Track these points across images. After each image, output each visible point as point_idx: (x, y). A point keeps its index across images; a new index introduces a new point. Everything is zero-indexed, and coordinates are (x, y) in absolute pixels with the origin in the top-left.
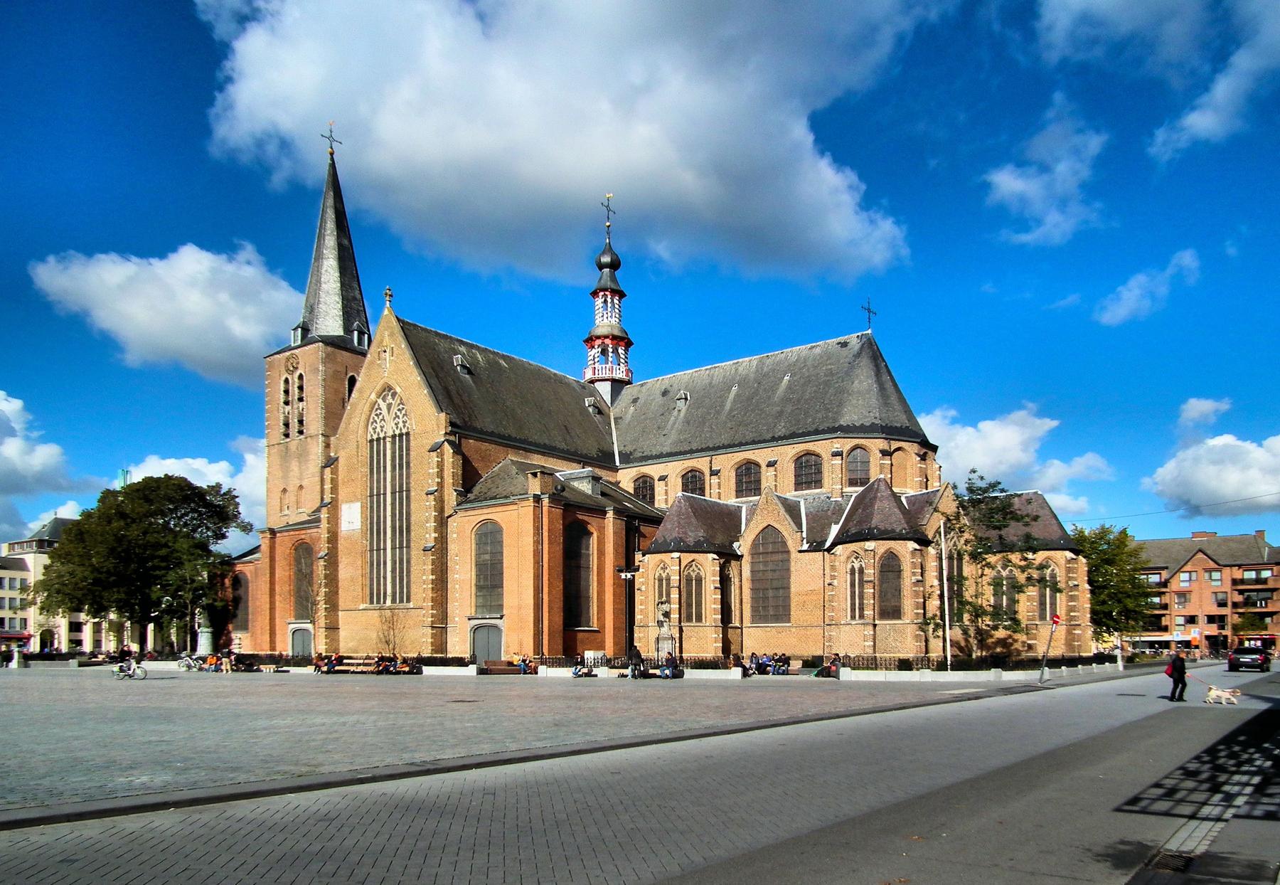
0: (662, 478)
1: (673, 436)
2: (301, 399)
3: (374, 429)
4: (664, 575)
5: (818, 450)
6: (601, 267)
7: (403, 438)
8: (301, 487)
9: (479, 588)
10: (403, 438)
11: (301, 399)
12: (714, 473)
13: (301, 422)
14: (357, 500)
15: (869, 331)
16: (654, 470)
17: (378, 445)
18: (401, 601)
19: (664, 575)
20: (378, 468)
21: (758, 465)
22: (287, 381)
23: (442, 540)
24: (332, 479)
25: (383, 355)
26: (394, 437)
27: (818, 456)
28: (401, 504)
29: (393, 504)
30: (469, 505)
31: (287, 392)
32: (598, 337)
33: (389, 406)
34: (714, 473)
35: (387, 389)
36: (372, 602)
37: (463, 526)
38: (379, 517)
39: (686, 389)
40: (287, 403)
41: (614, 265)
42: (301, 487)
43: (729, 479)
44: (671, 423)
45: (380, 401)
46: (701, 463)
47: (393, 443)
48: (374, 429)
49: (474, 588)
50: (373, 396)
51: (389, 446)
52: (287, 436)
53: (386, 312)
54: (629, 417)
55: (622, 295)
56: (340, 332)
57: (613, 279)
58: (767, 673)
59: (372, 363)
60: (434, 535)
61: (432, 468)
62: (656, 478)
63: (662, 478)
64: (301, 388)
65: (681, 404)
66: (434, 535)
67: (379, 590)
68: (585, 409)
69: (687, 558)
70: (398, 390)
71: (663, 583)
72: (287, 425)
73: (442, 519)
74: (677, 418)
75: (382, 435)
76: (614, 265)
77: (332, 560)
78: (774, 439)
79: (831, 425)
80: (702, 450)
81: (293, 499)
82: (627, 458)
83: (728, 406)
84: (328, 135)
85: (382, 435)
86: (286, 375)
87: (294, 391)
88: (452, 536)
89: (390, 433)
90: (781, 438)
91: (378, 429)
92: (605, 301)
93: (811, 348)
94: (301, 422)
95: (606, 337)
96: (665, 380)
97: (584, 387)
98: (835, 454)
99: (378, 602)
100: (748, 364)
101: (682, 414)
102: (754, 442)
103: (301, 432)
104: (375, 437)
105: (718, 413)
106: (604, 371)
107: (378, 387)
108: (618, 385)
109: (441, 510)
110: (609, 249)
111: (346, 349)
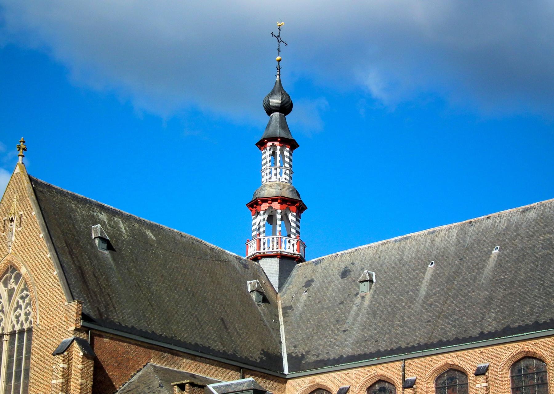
1: (356, 333)
6: (270, 110)
25: (9, 225)
26: (13, 334)
27: (541, 360)
32: (265, 200)
41: (285, 108)
44: (352, 314)
55: (293, 145)
65: (364, 288)
70: (23, 270)
74: (360, 308)
78: (483, 336)
83: (423, 290)
89: (9, 329)
92: (274, 154)
95: (274, 200)
96: (345, 256)
97: (246, 266)
101: (367, 303)
102: (457, 341)
105: (412, 300)
108: (288, 262)
110: (279, 89)
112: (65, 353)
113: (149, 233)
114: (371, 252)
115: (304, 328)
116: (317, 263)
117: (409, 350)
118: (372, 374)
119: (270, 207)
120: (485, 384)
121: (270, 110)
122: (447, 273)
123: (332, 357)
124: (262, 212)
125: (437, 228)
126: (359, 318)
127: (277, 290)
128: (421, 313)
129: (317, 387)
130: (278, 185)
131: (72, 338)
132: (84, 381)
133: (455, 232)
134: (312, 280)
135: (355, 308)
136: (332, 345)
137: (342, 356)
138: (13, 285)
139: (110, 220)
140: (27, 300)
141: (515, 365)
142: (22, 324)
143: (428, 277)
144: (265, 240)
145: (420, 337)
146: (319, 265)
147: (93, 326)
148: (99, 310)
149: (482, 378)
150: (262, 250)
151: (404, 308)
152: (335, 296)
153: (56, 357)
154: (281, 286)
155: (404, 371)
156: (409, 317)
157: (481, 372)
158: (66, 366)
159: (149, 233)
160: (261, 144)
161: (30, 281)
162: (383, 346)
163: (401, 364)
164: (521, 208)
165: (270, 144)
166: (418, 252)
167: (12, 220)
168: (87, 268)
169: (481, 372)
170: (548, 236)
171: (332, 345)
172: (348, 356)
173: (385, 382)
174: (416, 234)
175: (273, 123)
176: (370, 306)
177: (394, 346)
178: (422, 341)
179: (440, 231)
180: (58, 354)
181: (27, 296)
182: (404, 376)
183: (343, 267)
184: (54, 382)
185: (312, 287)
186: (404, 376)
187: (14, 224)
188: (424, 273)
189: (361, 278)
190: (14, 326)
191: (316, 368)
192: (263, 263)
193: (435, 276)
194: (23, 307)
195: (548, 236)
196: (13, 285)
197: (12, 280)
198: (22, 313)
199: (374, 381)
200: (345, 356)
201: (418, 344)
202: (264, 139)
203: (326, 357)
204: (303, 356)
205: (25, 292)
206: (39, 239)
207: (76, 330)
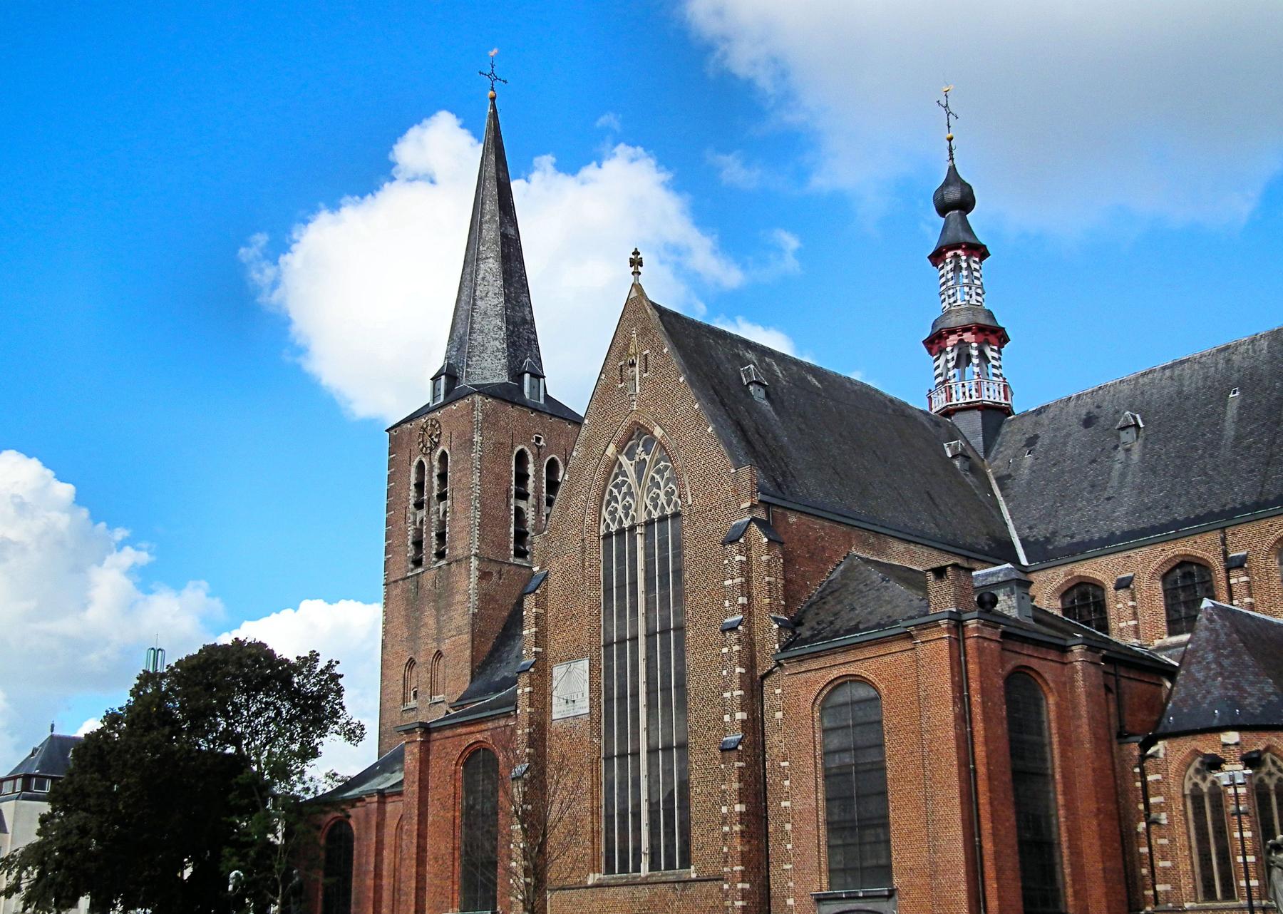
1: (1128, 500)
2: (442, 497)
3: (613, 513)
4: (1205, 787)
5: (1099, 576)
8: (439, 654)
9: (833, 827)
11: (442, 497)
12: (1233, 565)
13: (441, 537)
16: (1101, 569)
18: (670, 865)
19: (1205, 787)
21: (1098, 587)
23: (755, 727)
24: (537, 616)
26: (649, 524)
28: (666, 655)
29: (650, 659)
30: (806, 648)
31: (420, 486)
32: (952, 331)
36: (609, 869)
39: (1130, 408)
40: (419, 505)
42: (439, 654)
43: (1153, 595)
44: (1115, 474)
45: (623, 459)
46: (1203, 547)
47: (648, 536)
48: (613, 513)
49: (823, 830)
50: (611, 449)
51: (640, 542)
54: (1025, 472)
60: (740, 716)
61: (732, 583)
62: (1110, 586)
63: (1123, 584)
64: (443, 477)
66: (740, 716)
68: (949, 462)
69: (1258, 742)
70: (658, 432)
71: (1208, 809)
72: (418, 544)
73: (752, 680)
74: (1126, 466)
77: (537, 784)
81: (425, 677)
82: (1043, 553)
84: (488, 71)
89: (643, 517)
94: (441, 537)
97: (937, 424)
99: (624, 869)
101: (1135, 457)
103: (441, 555)
105: (1214, 445)
107: (620, 433)
109: (750, 664)
111: (514, 404)
112: (742, 540)
113: (810, 378)
115: (1040, 501)
118: (1170, 554)
119: (961, 341)
120: (1134, 622)
121: (943, 209)
122: (1264, 402)
124: (949, 349)
126: (1129, 478)
127: (982, 455)
128: (1235, 461)
129: (1077, 581)
130: (968, 309)
131: (747, 519)
132: (772, 579)
134: (1036, 437)
135: (1117, 466)
136: (1093, 521)
137: (1113, 533)
138: (643, 456)
139: (761, 361)
140: (667, 474)
141: (825, 704)
142: (621, 522)
143: (1232, 411)
145: (1241, 493)
146: (1044, 416)
147: (775, 502)
148: (775, 480)
150: (954, 402)
151: (1201, 457)
152: (1080, 454)
153: (728, 547)
154: (987, 450)
155: (1224, 544)
156: (1214, 469)
158: (744, 559)
159: (810, 378)
161: (671, 444)
162: (1180, 513)
165: (950, 254)
166: (1206, 378)
167: (633, 364)
168: (747, 423)
171: (1093, 521)
172: (1123, 532)
173: (1192, 563)
175: (952, 225)
176: (1143, 459)
178: (1248, 500)
180: (731, 542)
182: (1225, 553)
183: (1084, 412)
185: (1038, 446)
186: (1225, 553)
187: (637, 369)
188: (1225, 406)
189: (1121, 423)
190: (650, 513)
193: (865, 544)
194: (620, 498)
196: (643, 456)
197: (641, 448)
198: (620, 507)
199: (1173, 564)
200: (1118, 533)
201: (1243, 503)
202: (941, 248)
204: (1048, 540)
205: (620, 478)
206: (678, 385)
207: (752, 506)
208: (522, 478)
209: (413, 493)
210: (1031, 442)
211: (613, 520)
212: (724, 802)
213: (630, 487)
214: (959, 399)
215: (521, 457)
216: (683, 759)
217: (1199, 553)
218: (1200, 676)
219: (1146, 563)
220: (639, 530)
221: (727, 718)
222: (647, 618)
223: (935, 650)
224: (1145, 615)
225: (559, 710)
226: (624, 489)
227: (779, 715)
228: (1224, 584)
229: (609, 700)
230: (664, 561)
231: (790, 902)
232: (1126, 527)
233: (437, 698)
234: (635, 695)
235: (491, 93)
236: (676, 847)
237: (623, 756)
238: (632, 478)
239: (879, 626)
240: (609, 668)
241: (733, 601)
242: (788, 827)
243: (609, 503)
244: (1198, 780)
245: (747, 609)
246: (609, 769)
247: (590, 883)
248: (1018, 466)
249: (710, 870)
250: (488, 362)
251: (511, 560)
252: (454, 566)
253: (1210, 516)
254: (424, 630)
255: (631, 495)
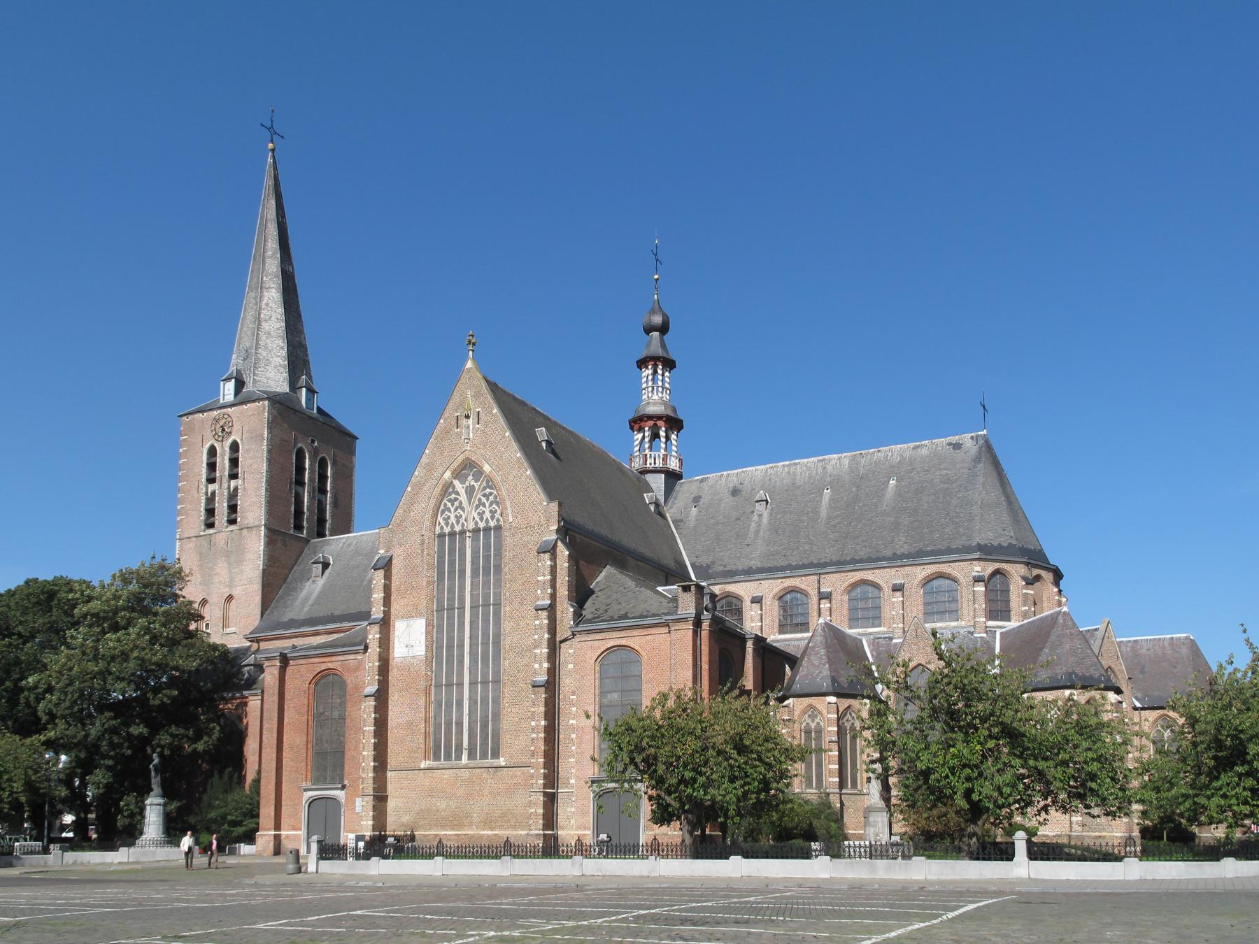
0: (757, 600)
3: (447, 519)
4: (813, 725)
5: (955, 573)
6: (648, 330)
7: (491, 534)
10: (491, 534)
11: (234, 476)
12: (824, 596)
14: (420, 615)
15: (985, 432)
17: (452, 542)
19: (813, 725)
20: (452, 572)
21: (739, 599)
22: (212, 452)
23: (553, 672)
25: (464, 422)
26: (476, 531)
27: (954, 580)
28: (486, 621)
32: (650, 417)
33: (470, 491)
34: (824, 596)
35: (468, 468)
37: (581, 656)
38: (450, 639)
41: (664, 329)
43: (772, 609)
45: (456, 482)
46: (807, 583)
50: (448, 475)
51: (468, 542)
52: (210, 525)
53: (469, 364)
55: (669, 364)
56: (284, 387)
57: (663, 346)
58: (1006, 853)
59: (447, 432)
65: (760, 507)
67: (448, 740)
69: (844, 703)
70: (487, 468)
75: (457, 528)
76: (664, 329)
78: (895, 557)
79: (966, 543)
80: (804, 566)
83: (824, 512)
84: (269, 125)
85: (457, 528)
86: (212, 442)
87: (223, 462)
88: (567, 667)
89: (471, 526)
90: (902, 557)
91: (453, 520)
92: (655, 372)
93: (915, 448)
95: (659, 417)
96: (733, 476)
98: (977, 580)
100: (838, 461)
101: (765, 520)
102: (870, 560)
103: (232, 522)
104: (447, 530)
106: (655, 459)
108: (673, 477)
109: (552, 629)
114: (759, 475)
116: (702, 481)
117: (825, 565)
123: (740, 568)
125: (827, 457)
133: (846, 462)
134: (700, 497)
135: (753, 525)
138: (473, 483)
140: (491, 498)
142: (487, 521)
144: (645, 454)
145: (830, 554)
149: (899, 593)
157: (898, 588)
160: (642, 363)
161: (498, 478)
163: (816, 577)
164: (912, 445)
166: (810, 477)
167: (468, 417)
169: (898, 588)
170: (944, 472)
174: (805, 461)
177: (806, 561)
178: (835, 558)
179: (830, 460)
181: (491, 494)
184: (540, 578)
187: (470, 421)
189: (757, 498)
190: (476, 523)
191: (725, 577)
192: (649, 477)
195: (944, 472)
196: (473, 483)
203: (734, 568)
204: (708, 566)
208: (300, 469)
209: (204, 470)
210: (697, 500)
211: (447, 524)
212: (533, 719)
213: (461, 503)
214: (650, 464)
215: (300, 455)
216: (497, 691)
217: (803, 587)
218: (816, 662)
219: (770, 588)
220: (468, 534)
221: (537, 666)
222: (472, 595)
223: (685, 633)
224: (767, 621)
225: (399, 651)
226: (456, 504)
227: (571, 666)
228: (816, 607)
229: (440, 648)
230: (487, 558)
231: (572, 781)
232: (759, 565)
233: (228, 630)
234: (461, 646)
235: (271, 146)
236: (488, 744)
237: (449, 685)
238: (463, 498)
239: (641, 616)
240: (440, 627)
241: (543, 589)
242: (574, 736)
243: (443, 512)
244: (809, 721)
245: (553, 597)
246: (439, 693)
247: (422, 766)
248: (688, 515)
249: (515, 761)
250: (271, 373)
251: (292, 532)
252: (245, 532)
253: (811, 565)
254: (216, 579)
255: (463, 509)
